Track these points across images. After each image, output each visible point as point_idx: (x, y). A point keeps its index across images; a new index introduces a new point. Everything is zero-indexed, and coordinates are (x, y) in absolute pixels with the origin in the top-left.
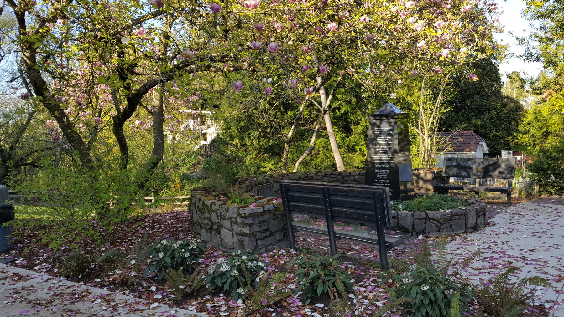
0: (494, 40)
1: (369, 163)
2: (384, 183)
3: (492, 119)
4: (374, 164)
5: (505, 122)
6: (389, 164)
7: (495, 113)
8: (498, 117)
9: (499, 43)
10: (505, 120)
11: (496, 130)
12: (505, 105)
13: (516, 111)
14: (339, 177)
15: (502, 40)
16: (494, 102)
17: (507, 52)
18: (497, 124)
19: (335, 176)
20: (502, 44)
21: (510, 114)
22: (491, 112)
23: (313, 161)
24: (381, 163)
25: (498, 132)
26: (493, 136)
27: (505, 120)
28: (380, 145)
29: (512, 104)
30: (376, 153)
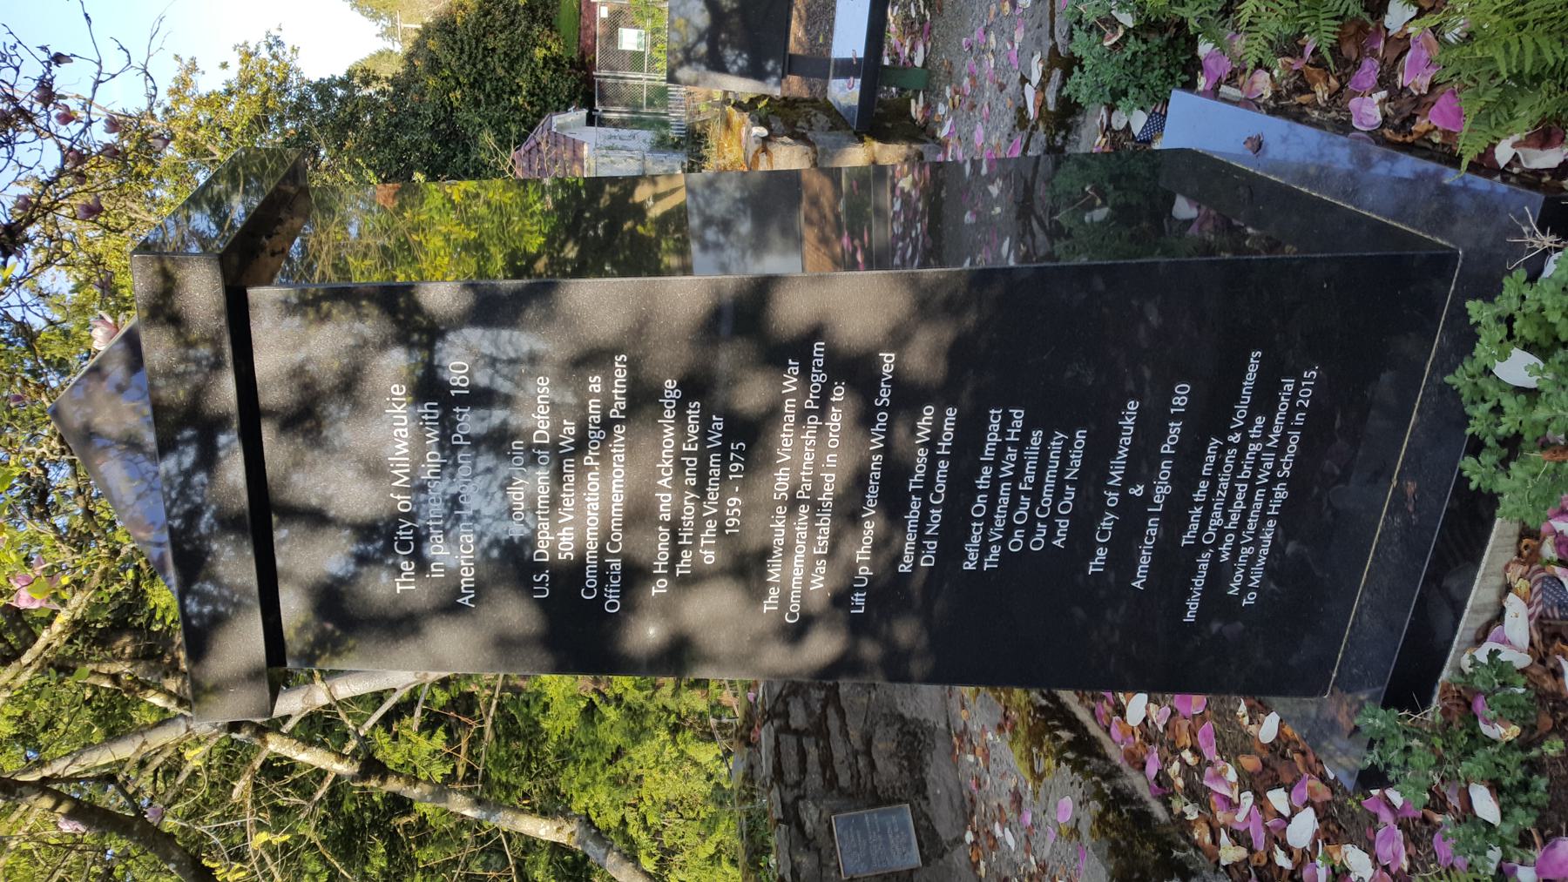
0: (221, 88)
1: (870, 650)
2: (1142, 464)
3: (477, 103)
4: (889, 591)
5: (486, 64)
6: (909, 397)
7: (458, 93)
8: (472, 86)
9: (233, 74)
10: (480, 66)
11: (513, 93)
12: (434, 65)
13: (453, 32)
14: (798, 718)
15: (224, 65)
16: (423, 95)
17: (264, 54)
18: (494, 90)
19: (789, 742)
20: (235, 61)
21: (462, 51)
22: (456, 104)
23: (628, 698)
24: (893, 506)
25: (520, 87)
26: (531, 103)
27: (480, 66)
28: (639, 514)
29: (433, 44)
30: (747, 567)
